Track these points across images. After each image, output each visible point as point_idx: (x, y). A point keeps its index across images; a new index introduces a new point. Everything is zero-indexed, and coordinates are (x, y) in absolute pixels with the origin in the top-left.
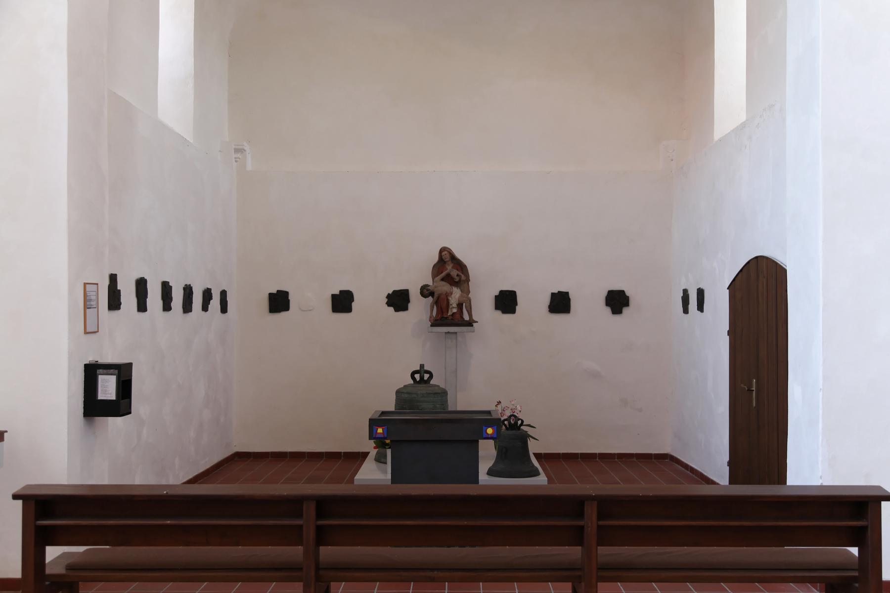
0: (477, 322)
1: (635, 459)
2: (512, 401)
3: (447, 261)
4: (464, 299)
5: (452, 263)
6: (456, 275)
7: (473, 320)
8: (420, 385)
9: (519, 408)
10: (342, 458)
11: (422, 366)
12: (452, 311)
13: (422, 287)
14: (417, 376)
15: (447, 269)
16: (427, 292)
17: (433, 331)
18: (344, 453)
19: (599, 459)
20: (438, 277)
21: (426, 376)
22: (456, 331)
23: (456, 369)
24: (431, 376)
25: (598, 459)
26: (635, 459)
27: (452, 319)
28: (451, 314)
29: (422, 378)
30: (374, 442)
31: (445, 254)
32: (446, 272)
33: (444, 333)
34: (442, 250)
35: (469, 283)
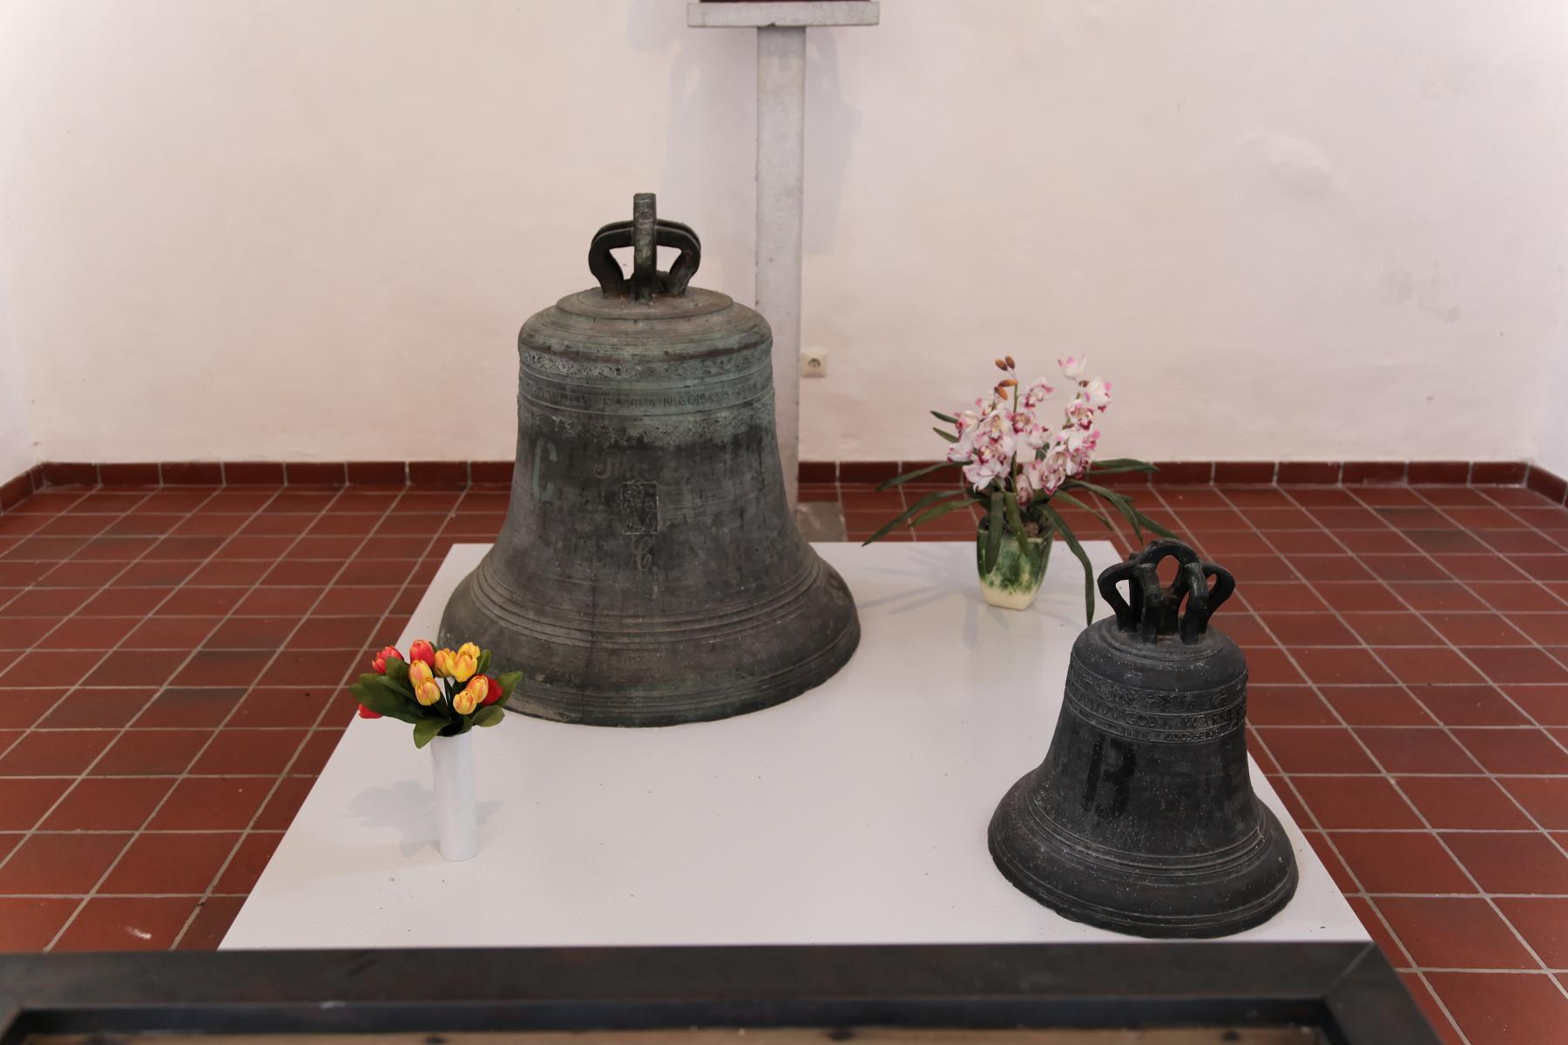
1: (1404, 484)
2: (1070, 360)
8: (638, 310)
9: (1102, 391)
10: (408, 483)
11: (645, 204)
14: (625, 258)
17: (711, 23)
18: (414, 466)
19: (1279, 481)
21: (666, 258)
22: (800, 23)
23: (801, 180)
24: (690, 258)
25: (1274, 484)
26: (1404, 484)
29: (646, 270)
30: (365, 715)
33: (755, 30)
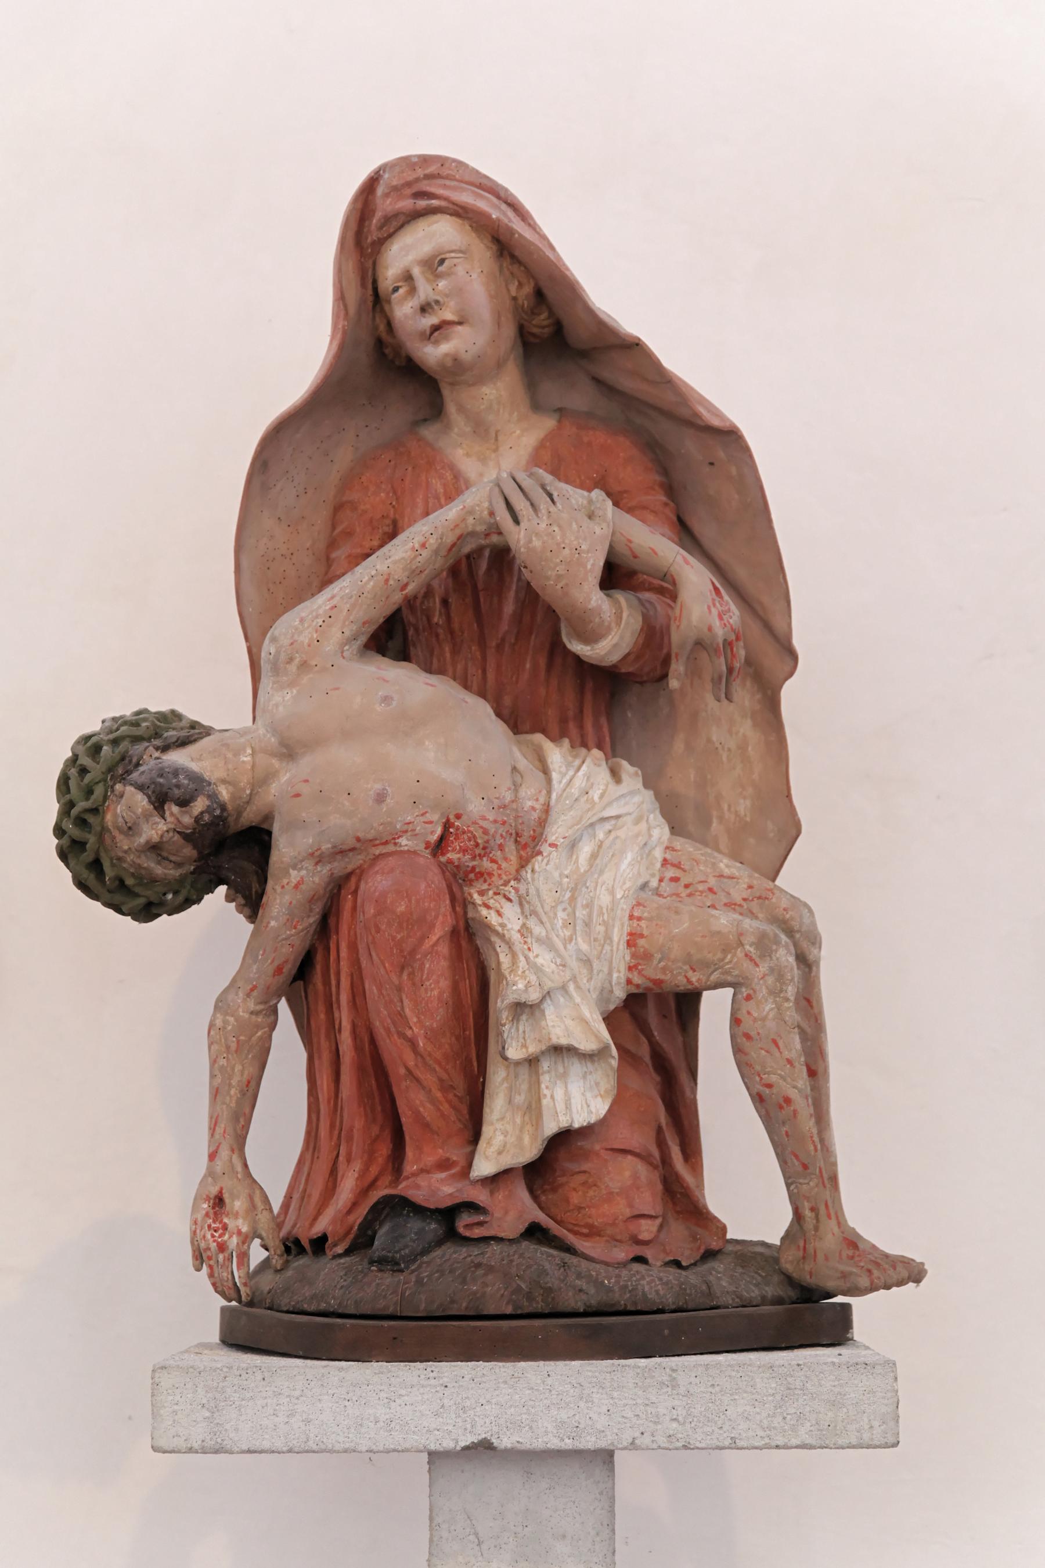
0: (914, 1273)
3: (457, 367)
4: (724, 920)
5: (536, 406)
6: (596, 563)
7: (852, 1242)
12: (534, 1110)
13: (89, 745)
15: (456, 487)
16: (154, 829)
20: (321, 602)
27: (534, 1232)
28: (529, 1151)
31: (434, 264)
32: (450, 512)
34: (385, 205)
35: (790, 694)
